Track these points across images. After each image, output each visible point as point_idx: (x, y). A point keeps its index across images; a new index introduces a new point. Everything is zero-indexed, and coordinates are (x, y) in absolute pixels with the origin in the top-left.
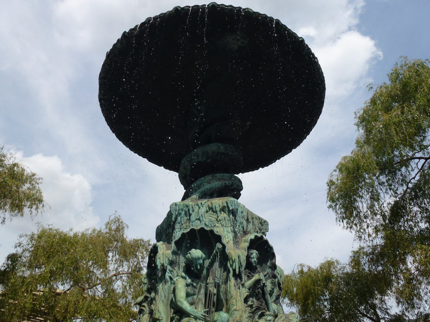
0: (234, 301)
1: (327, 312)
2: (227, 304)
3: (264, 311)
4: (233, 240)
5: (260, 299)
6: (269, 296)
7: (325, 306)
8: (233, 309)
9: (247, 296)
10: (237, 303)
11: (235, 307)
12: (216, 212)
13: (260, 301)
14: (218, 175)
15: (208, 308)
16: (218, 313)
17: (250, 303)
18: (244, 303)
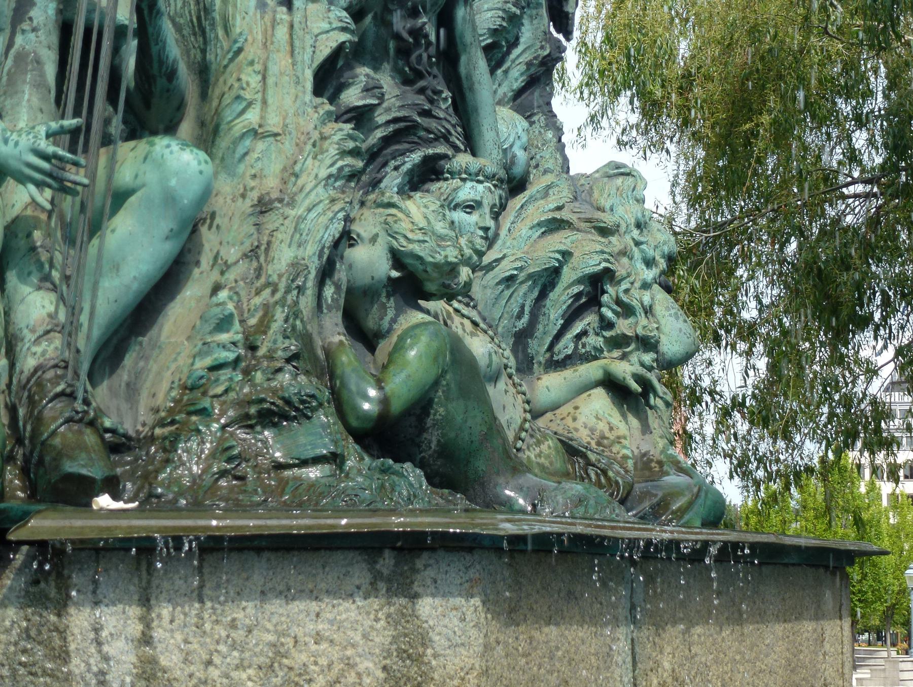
0: (254, 80)
1: (860, 188)
2: (204, 95)
3: (441, 149)
5: (419, 75)
6: (482, 64)
7: (853, 156)
8: (239, 127)
9: (339, 50)
10: (270, 92)
11: (252, 117)
13: (422, 91)
15: (77, 113)
16: (142, 146)
17: (353, 97)
18: (318, 91)
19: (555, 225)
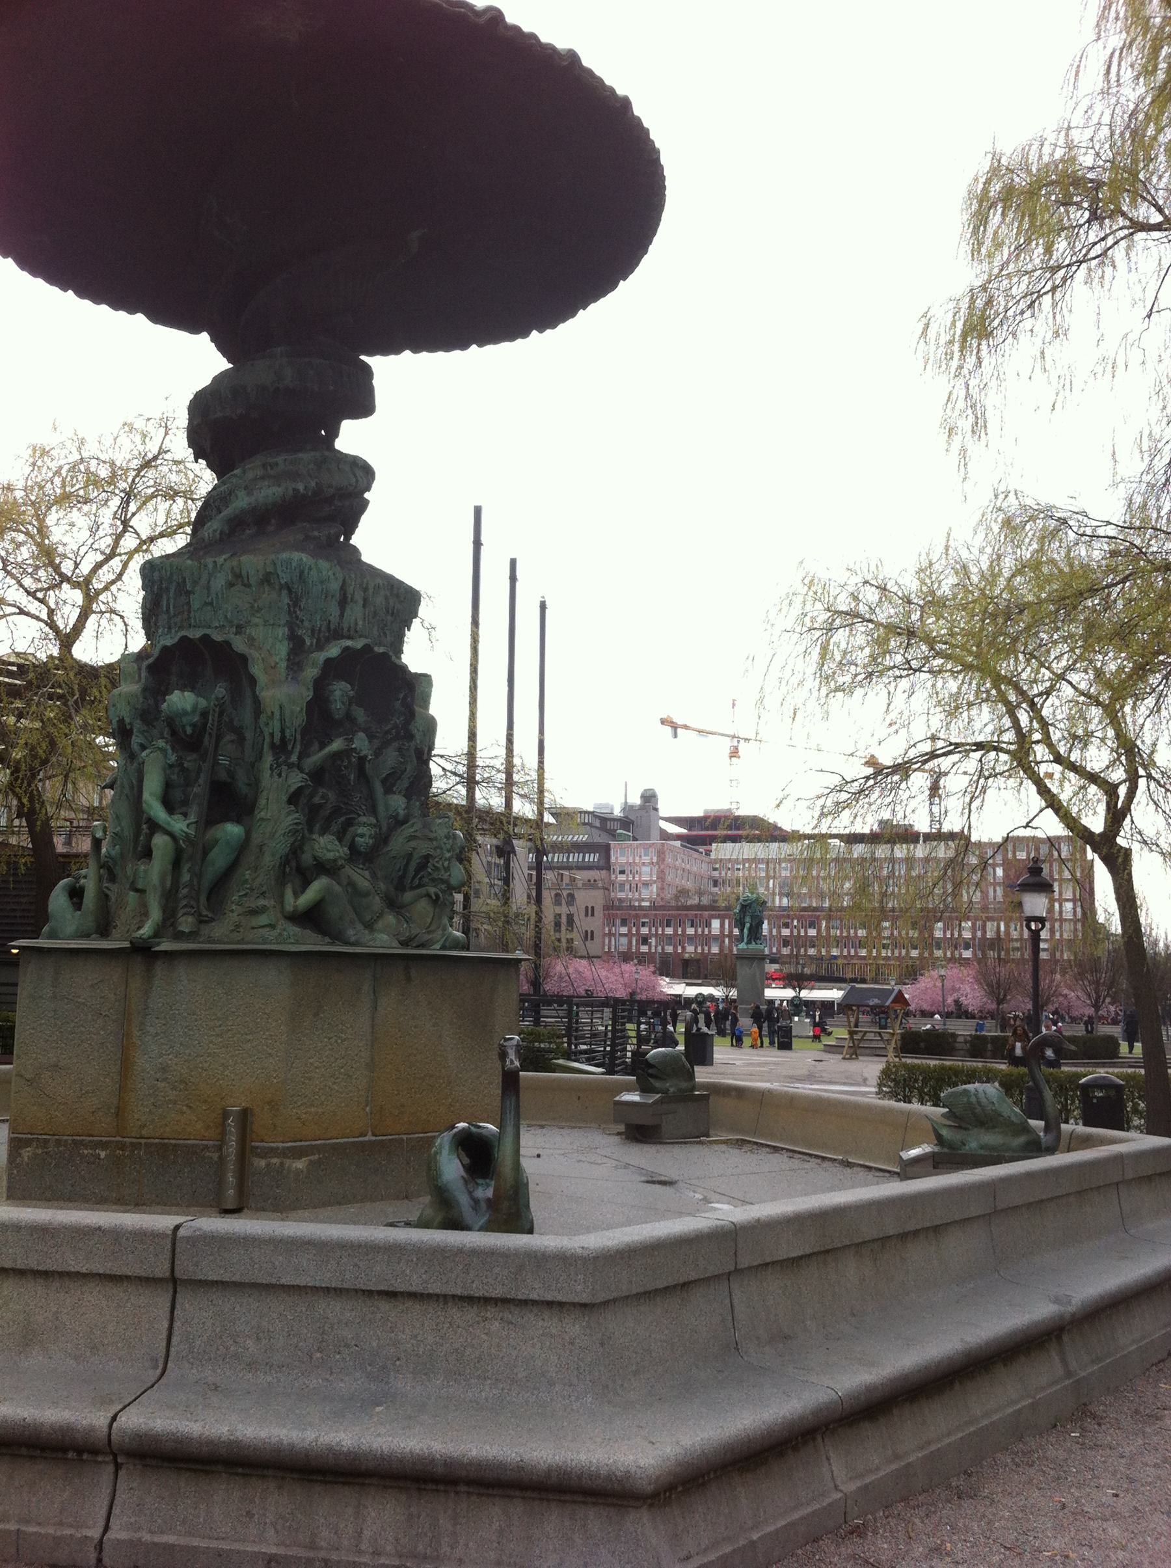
4: (288, 660)
12: (249, 586)
14: (280, 459)
19: (411, 838)
